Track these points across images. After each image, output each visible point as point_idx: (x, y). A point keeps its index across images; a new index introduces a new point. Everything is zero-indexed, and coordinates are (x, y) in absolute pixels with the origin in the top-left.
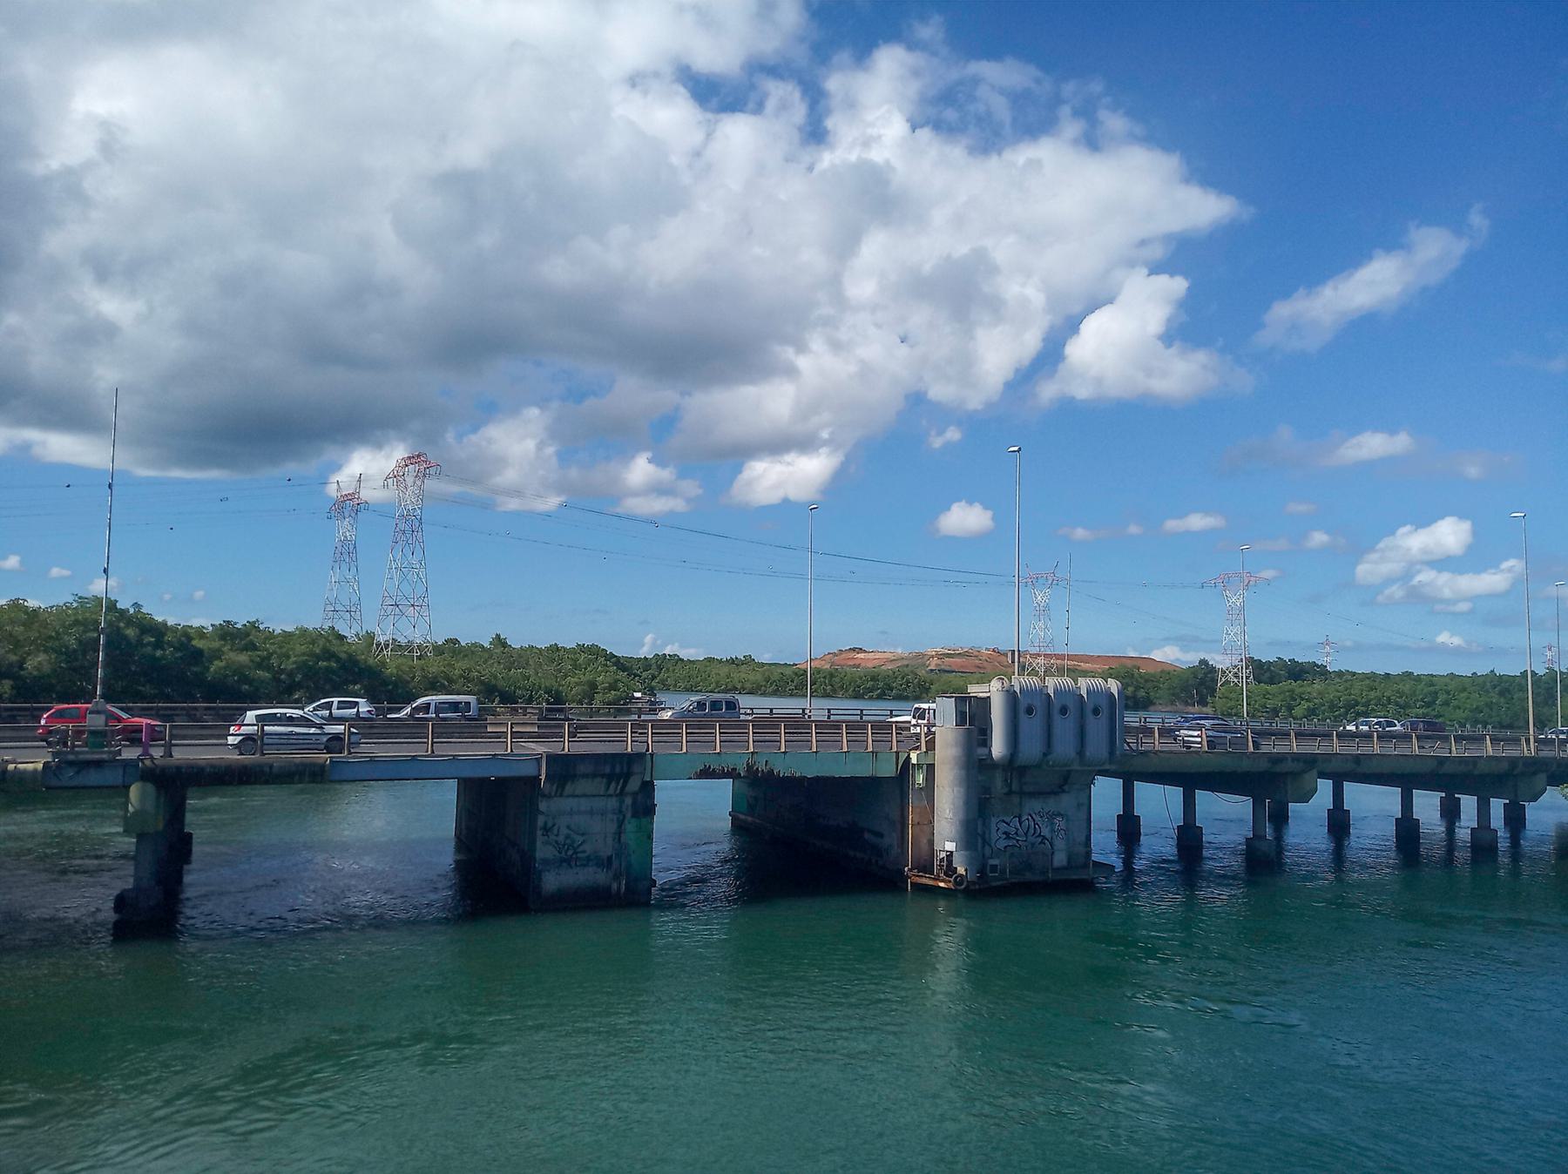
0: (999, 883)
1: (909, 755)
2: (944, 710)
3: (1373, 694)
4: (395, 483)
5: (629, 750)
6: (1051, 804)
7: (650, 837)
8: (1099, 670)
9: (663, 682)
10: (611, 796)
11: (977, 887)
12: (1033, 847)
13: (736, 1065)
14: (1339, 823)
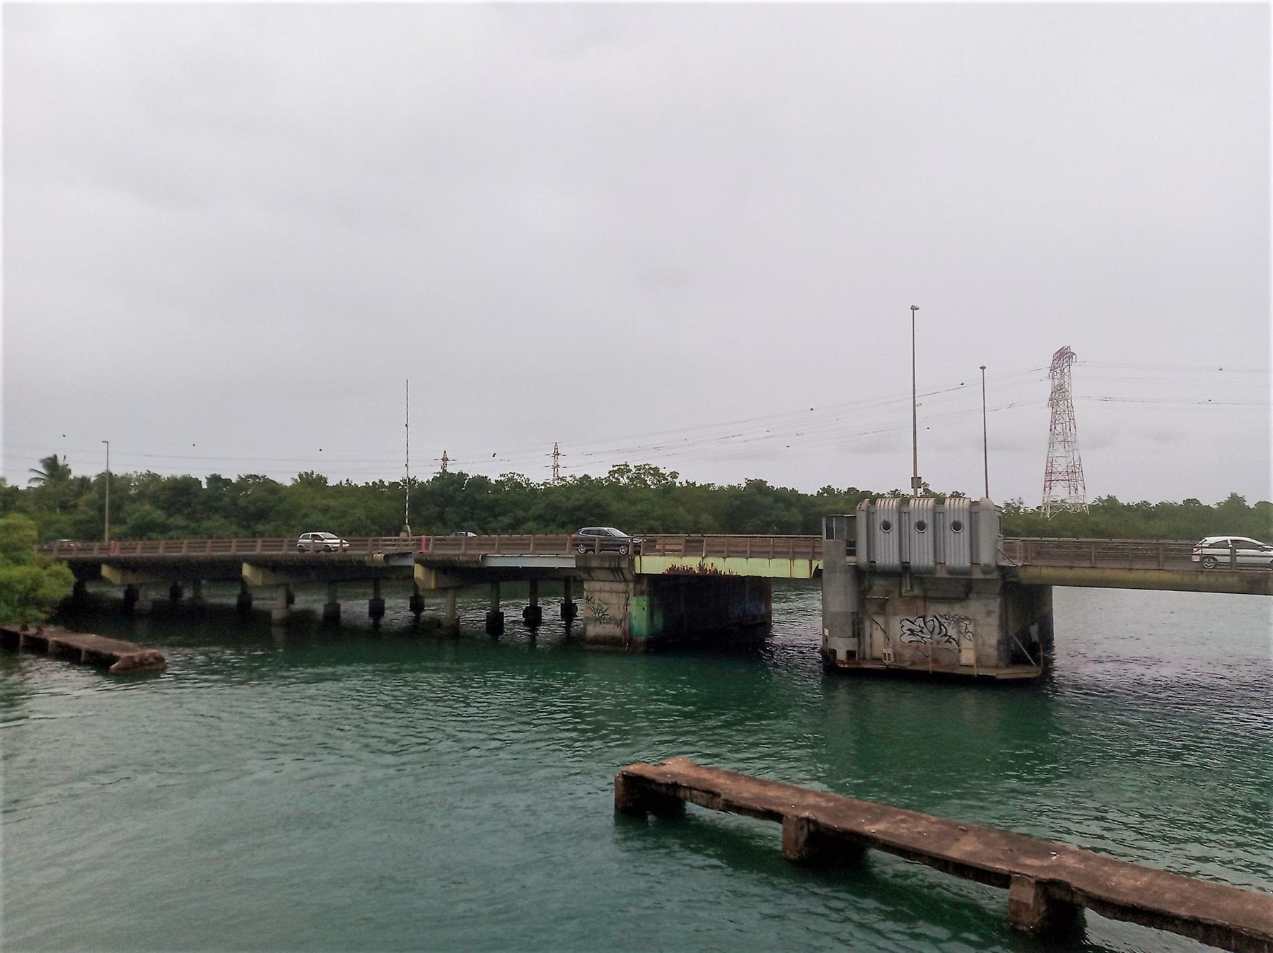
6: (958, 610)
13: (96, 786)
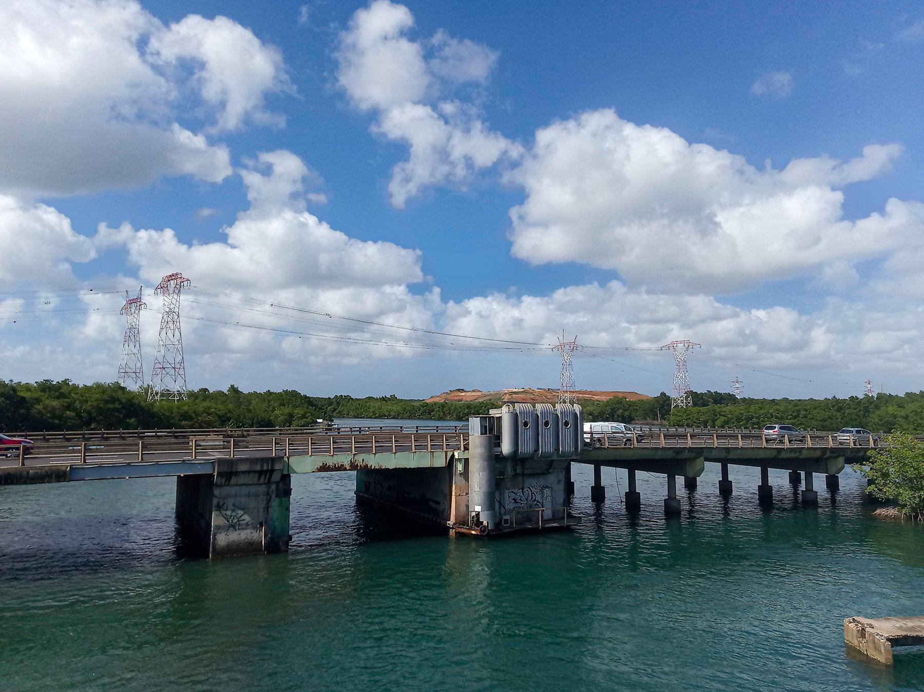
0: (508, 530)
1: (453, 453)
2: (475, 423)
3: (762, 412)
4: (162, 292)
5: (274, 455)
6: (542, 481)
7: (288, 509)
8: (604, 400)
9: (340, 412)
10: (262, 484)
11: (495, 533)
12: (531, 507)
14: (725, 488)
